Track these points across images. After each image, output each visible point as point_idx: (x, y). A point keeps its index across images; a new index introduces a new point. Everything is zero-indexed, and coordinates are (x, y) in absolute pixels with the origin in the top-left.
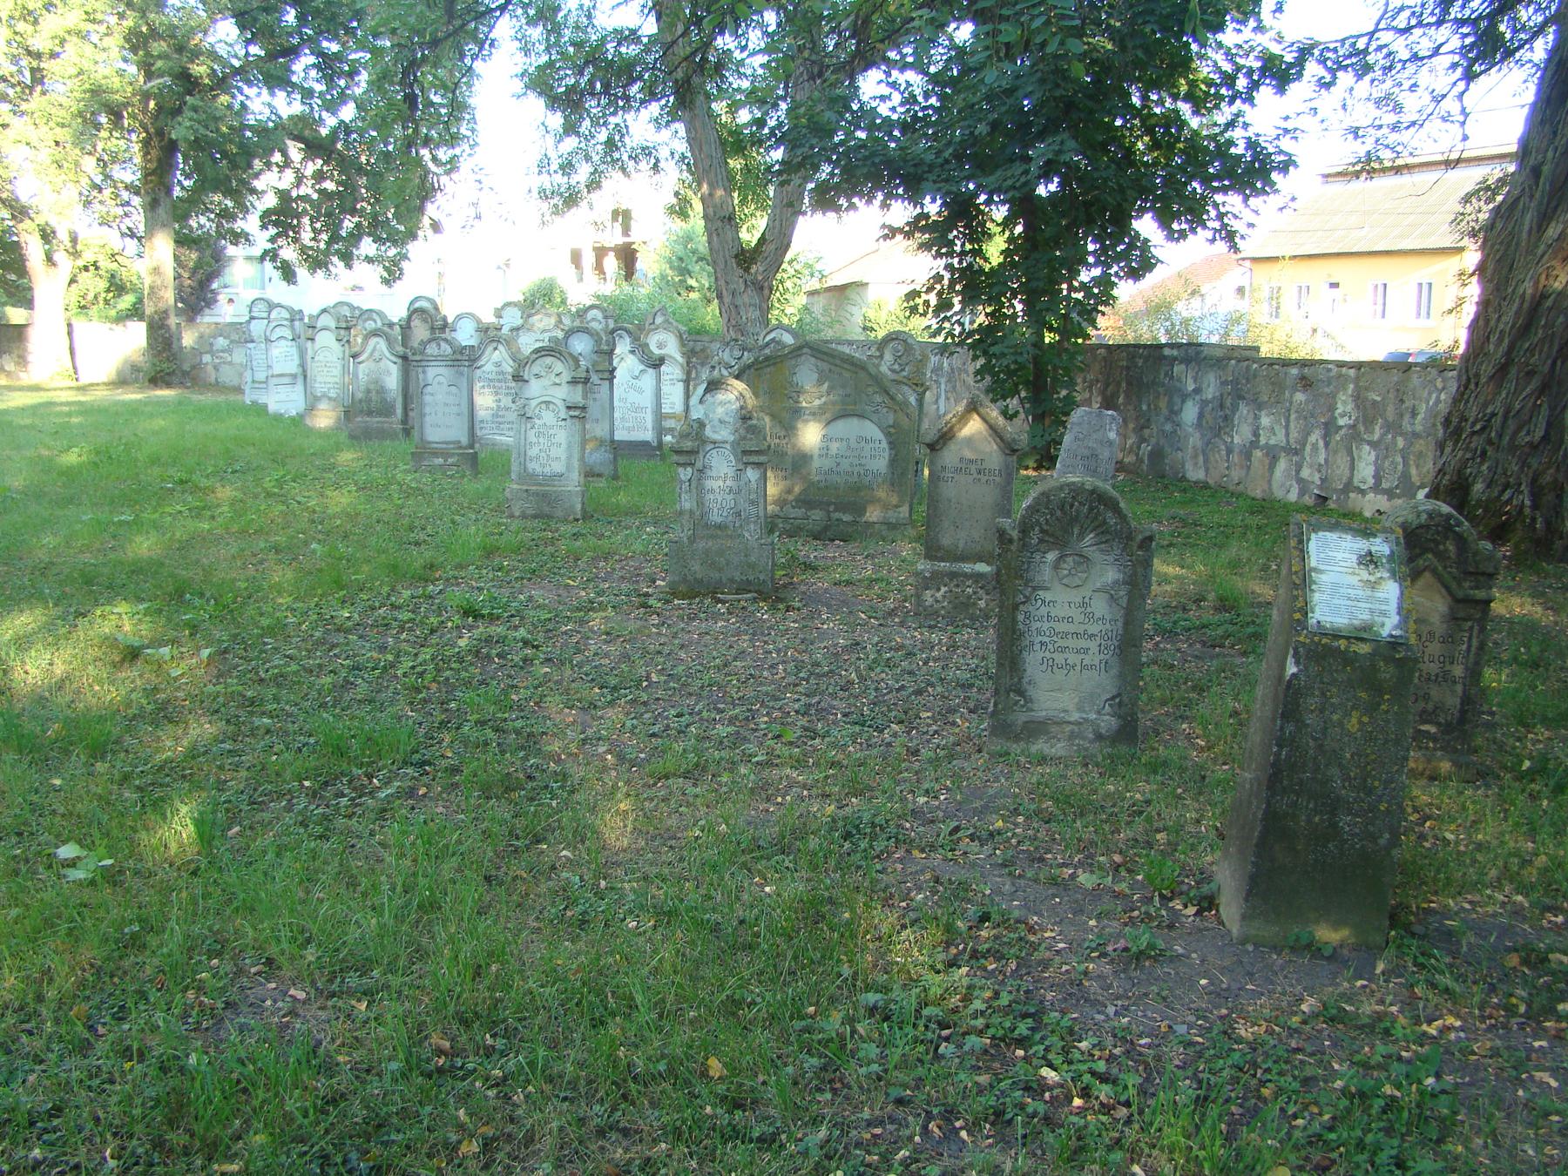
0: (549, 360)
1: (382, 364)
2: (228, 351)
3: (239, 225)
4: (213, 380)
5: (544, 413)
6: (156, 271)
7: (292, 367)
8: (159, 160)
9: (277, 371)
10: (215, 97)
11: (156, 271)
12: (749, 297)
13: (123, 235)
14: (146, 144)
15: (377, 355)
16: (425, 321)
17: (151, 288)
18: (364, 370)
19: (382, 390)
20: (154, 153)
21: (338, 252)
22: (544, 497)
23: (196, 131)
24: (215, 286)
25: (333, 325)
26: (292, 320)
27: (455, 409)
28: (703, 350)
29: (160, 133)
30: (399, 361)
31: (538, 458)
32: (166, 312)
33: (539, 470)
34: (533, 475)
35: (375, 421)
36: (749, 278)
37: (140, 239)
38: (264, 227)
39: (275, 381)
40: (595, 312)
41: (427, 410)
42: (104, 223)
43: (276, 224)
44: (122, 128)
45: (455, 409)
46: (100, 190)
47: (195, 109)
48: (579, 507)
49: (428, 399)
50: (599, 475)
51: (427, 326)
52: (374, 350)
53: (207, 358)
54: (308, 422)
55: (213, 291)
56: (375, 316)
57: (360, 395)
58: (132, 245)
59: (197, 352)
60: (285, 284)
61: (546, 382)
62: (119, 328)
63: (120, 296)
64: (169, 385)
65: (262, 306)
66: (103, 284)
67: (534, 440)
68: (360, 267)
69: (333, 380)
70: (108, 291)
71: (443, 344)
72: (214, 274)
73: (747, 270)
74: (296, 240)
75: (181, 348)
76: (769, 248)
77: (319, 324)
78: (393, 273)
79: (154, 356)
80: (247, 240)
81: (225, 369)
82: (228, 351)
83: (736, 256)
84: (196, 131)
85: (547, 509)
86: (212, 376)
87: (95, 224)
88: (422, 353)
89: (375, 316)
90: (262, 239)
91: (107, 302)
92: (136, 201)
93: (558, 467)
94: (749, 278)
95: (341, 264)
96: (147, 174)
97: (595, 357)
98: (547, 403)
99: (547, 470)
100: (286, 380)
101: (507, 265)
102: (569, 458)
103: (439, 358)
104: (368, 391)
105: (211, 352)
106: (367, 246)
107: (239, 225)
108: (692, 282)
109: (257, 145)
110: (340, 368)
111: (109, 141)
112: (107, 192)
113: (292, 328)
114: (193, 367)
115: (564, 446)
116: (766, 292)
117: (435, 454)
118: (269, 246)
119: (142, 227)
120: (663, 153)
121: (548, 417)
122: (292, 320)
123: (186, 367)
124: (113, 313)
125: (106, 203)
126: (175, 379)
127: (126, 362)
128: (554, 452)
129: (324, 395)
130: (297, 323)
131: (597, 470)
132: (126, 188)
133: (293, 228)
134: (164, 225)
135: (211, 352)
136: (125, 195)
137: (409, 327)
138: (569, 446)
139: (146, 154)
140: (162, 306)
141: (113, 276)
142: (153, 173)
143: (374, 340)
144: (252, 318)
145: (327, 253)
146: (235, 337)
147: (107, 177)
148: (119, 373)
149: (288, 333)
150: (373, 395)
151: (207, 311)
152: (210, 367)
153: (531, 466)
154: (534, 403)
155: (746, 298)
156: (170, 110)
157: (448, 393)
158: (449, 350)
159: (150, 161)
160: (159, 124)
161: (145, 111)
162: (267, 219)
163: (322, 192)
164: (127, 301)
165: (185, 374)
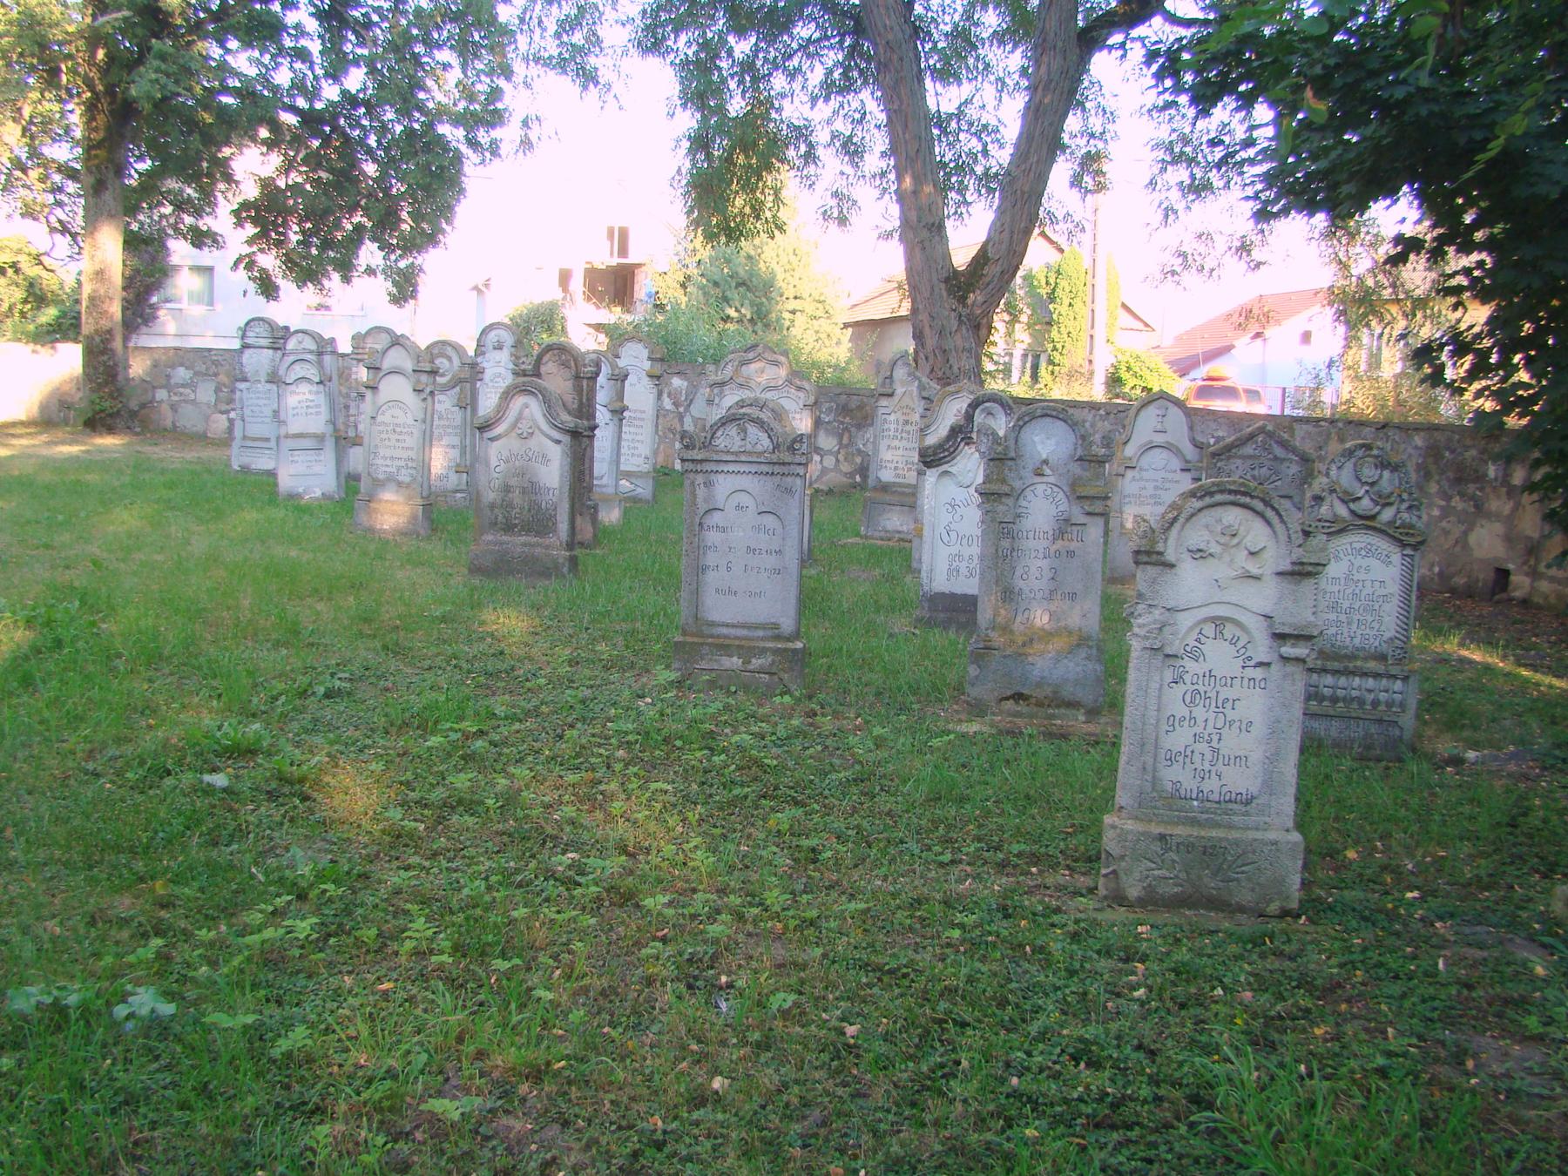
0: (1232, 516)
1: (532, 443)
2: (191, 385)
3: (207, 223)
5: (1209, 647)
6: (100, 275)
7: (317, 423)
8: (108, 128)
9: (294, 428)
10: (189, 44)
11: (100, 275)
12: (961, 339)
13: (53, 230)
14: (91, 109)
15: (524, 426)
16: (565, 365)
17: (92, 299)
18: (498, 454)
19: (532, 489)
20: (101, 120)
21: (334, 262)
22: (1209, 853)
23: (163, 87)
24: (154, 299)
25: (409, 365)
26: (320, 354)
27: (771, 561)
28: (860, 407)
29: (110, 91)
30: (566, 439)
31: (1187, 755)
32: (110, 332)
33: (1189, 784)
34: (1175, 799)
35: (518, 543)
36: (964, 312)
37: (74, 236)
38: (240, 224)
39: (291, 443)
41: (711, 559)
42: (29, 213)
43: (255, 222)
44: (58, 87)
45: (771, 561)
46: (24, 170)
47: (163, 57)
48: (1295, 880)
49: (712, 537)
50: (1072, 705)
51: (568, 374)
52: (519, 419)
53: (161, 394)
55: (152, 306)
56: (449, 351)
57: (490, 496)
58: (63, 242)
59: (148, 385)
60: (262, 299)
61: (1218, 570)
62: (45, 351)
63: (39, 308)
64: (111, 430)
65: (261, 329)
66: (19, 294)
67: (1181, 711)
68: (360, 283)
69: (405, 455)
70: (25, 301)
71: (752, 430)
73: (962, 300)
74: (279, 244)
75: (128, 380)
76: (992, 271)
77: (387, 364)
78: (405, 288)
79: (92, 391)
80: (215, 241)
81: (187, 410)
82: (191, 385)
83: (947, 280)
84: (163, 87)
85: (1211, 884)
86: (168, 419)
87: (17, 216)
88: (707, 445)
89: (449, 351)
90: (237, 239)
91: (23, 314)
92: (72, 187)
93: (1241, 781)
94: (964, 312)
95: (336, 276)
96: (90, 147)
97: (1076, 469)
98: (1219, 622)
99: (1211, 785)
100: (308, 443)
101: (487, 286)
102: (1273, 759)
103: (737, 458)
104: (507, 489)
106: (370, 253)
107: (207, 223)
108: (732, 313)
109: (239, 112)
110: (417, 433)
111: (36, 102)
112: (34, 174)
113: (320, 364)
114: (143, 406)
115: (1259, 729)
116: (983, 331)
117: (725, 648)
118: (246, 250)
119: (80, 221)
120: (821, 136)
121: (1220, 657)
122: (320, 354)
124: (32, 327)
125: (33, 188)
126: (120, 423)
127: (52, 394)
128: (1232, 743)
129: (391, 479)
130: (327, 359)
131: (1067, 692)
132: (59, 170)
133: (276, 226)
134: (111, 216)
136: (57, 178)
138: (1274, 731)
139: (88, 122)
140: (105, 324)
141: (31, 285)
142: (99, 145)
143: (519, 401)
144: (245, 346)
145: (319, 260)
147: (34, 153)
148: (44, 407)
149: (312, 372)
150: (516, 498)
151: (144, 329)
152: (165, 407)
153: (1177, 776)
154: (1185, 621)
155: (958, 341)
156: (121, 65)
157: (757, 528)
158: (766, 442)
159: (96, 130)
160: (113, 79)
161: (91, 61)
162: (242, 214)
163: (317, 182)
164: (49, 314)
165: (133, 414)
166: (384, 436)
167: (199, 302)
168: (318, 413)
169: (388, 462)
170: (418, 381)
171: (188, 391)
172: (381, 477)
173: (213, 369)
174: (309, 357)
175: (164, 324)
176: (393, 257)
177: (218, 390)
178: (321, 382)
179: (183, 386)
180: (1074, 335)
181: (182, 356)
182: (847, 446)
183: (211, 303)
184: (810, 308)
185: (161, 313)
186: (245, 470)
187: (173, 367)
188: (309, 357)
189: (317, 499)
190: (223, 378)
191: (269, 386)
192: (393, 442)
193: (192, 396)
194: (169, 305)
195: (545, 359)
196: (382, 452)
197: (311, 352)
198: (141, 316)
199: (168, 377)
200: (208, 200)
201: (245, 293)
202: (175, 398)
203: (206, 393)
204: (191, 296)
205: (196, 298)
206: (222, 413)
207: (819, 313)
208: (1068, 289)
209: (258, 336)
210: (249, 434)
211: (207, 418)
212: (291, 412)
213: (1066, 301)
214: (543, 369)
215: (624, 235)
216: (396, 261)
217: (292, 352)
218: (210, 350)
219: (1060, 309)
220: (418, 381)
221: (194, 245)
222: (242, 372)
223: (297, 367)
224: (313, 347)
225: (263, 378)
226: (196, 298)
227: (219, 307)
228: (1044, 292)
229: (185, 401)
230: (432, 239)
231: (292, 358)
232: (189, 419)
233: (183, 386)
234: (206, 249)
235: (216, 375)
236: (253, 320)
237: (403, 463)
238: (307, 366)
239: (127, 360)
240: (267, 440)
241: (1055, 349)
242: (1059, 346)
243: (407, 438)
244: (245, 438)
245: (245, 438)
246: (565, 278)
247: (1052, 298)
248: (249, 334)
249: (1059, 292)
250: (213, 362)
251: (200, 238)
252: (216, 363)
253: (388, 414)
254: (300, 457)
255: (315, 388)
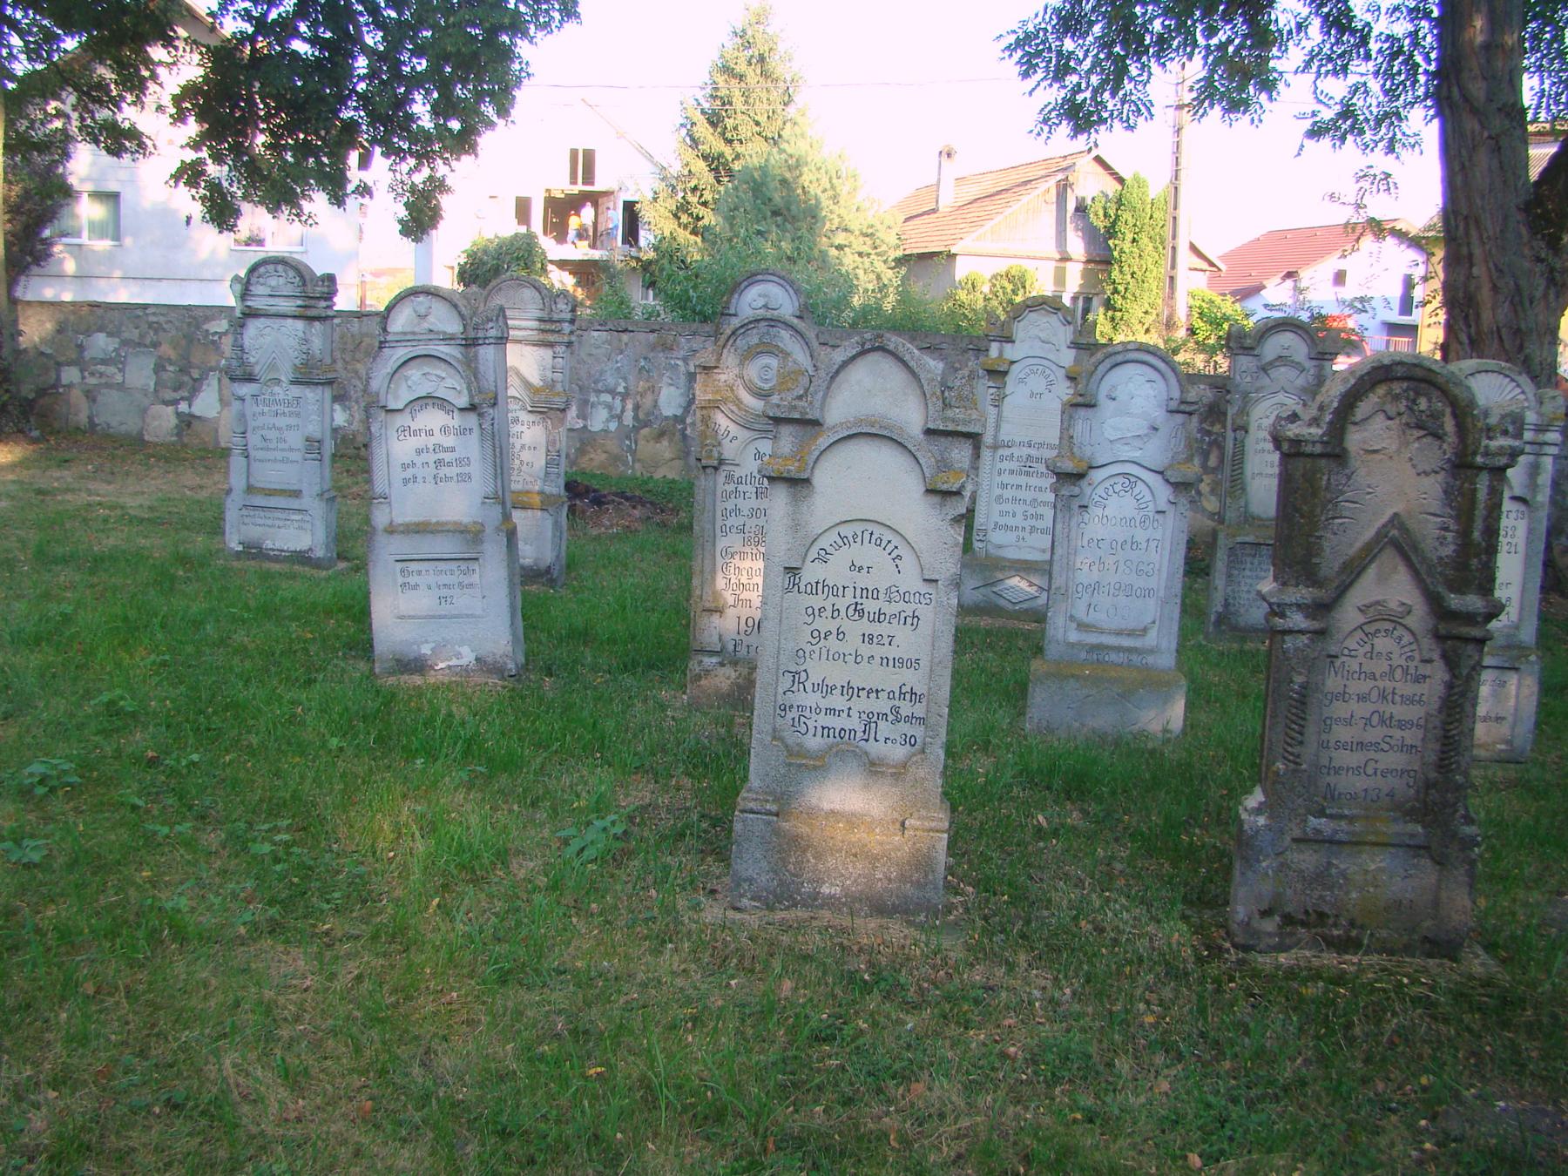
4: (82, 419)
24: (47, 233)
38: (179, 118)
40: (1287, 339)
51: (1434, 455)
53: (70, 375)
54: (19, 307)
59: (48, 360)
65: (279, 281)
69: (892, 679)
72: (46, 215)
75: (18, 353)
81: (109, 398)
100: (445, 546)
105: (80, 362)
107: (129, 115)
114: (42, 392)
118: (190, 156)
122: (470, 343)
123: (27, 390)
135: (80, 362)
137: (1335, 453)
144: (251, 314)
146: (132, 333)
151: (35, 270)
152: (77, 396)
166: (823, 624)
167: (102, 236)
168: (464, 478)
169: (838, 701)
170: (943, 465)
171: (112, 370)
172: (814, 742)
173: (151, 337)
174: (443, 350)
175: (61, 261)
176: (405, 167)
177: (159, 368)
178: (472, 408)
179: (104, 362)
180: (1139, 274)
181: (99, 315)
182: (1214, 470)
183: (117, 237)
184: (859, 244)
185: (57, 249)
186: (253, 551)
187: (88, 332)
188: (443, 350)
189: (465, 670)
190: (167, 350)
191: (296, 391)
192: (853, 643)
193: (119, 378)
194: (65, 240)
195: (1363, 409)
196: (818, 671)
197: (448, 339)
198: (31, 254)
199: (81, 348)
200: (135, 84)
201: (189, 220)
202: (93, 381)
203: (140, 373)
204: (92, 225)
205: (98, 230)
206: (167, 403)
207: (866, 249)
208: (1131, 221)
209: (275, 293)
210: (259, 481)
211: (144, 412)
212: (398, 475)
213: (1129, 237)
214: (1354, 439)
215: (589, 156)
216: (410, 172)
217: (407, 338)
218: (145, 307)
219: (1121, 245)
220: (943, 465)
221: (109, 151)
222: (243, 363)
223: (414, 373)
224: (454, 327)
225: (286, 374)
226: (98, 230)
227: (128, 241)
228: (1100, 223)
229: (108, 386)
230: (464, 143)
231: (401, 353)
232: (115, 414)
233: (104, 362)
234: (127, 157)
235: (156, 345)
236: (264, 262)
237: (883, 705)
238: (440, 370)
239: (15, 322)
240: (296, 494)
241: (1116, 291)
242: (1121, 288)
243: (902, 633)
244: (250, 489)
245: (250, 489)
246: (523, 209)
247: (1111, 232)
248: (257, 289)
249: (1120, 226)
250: (150, 325)
251: (120, 141)
252: (157, 328)
253: (840, 559)
254: (427, 576)
255: (455, 421)
